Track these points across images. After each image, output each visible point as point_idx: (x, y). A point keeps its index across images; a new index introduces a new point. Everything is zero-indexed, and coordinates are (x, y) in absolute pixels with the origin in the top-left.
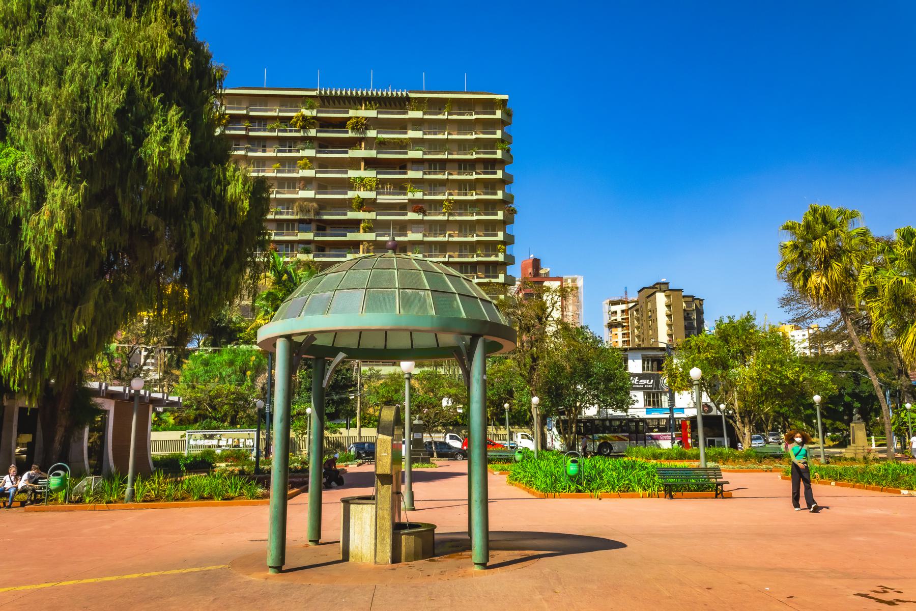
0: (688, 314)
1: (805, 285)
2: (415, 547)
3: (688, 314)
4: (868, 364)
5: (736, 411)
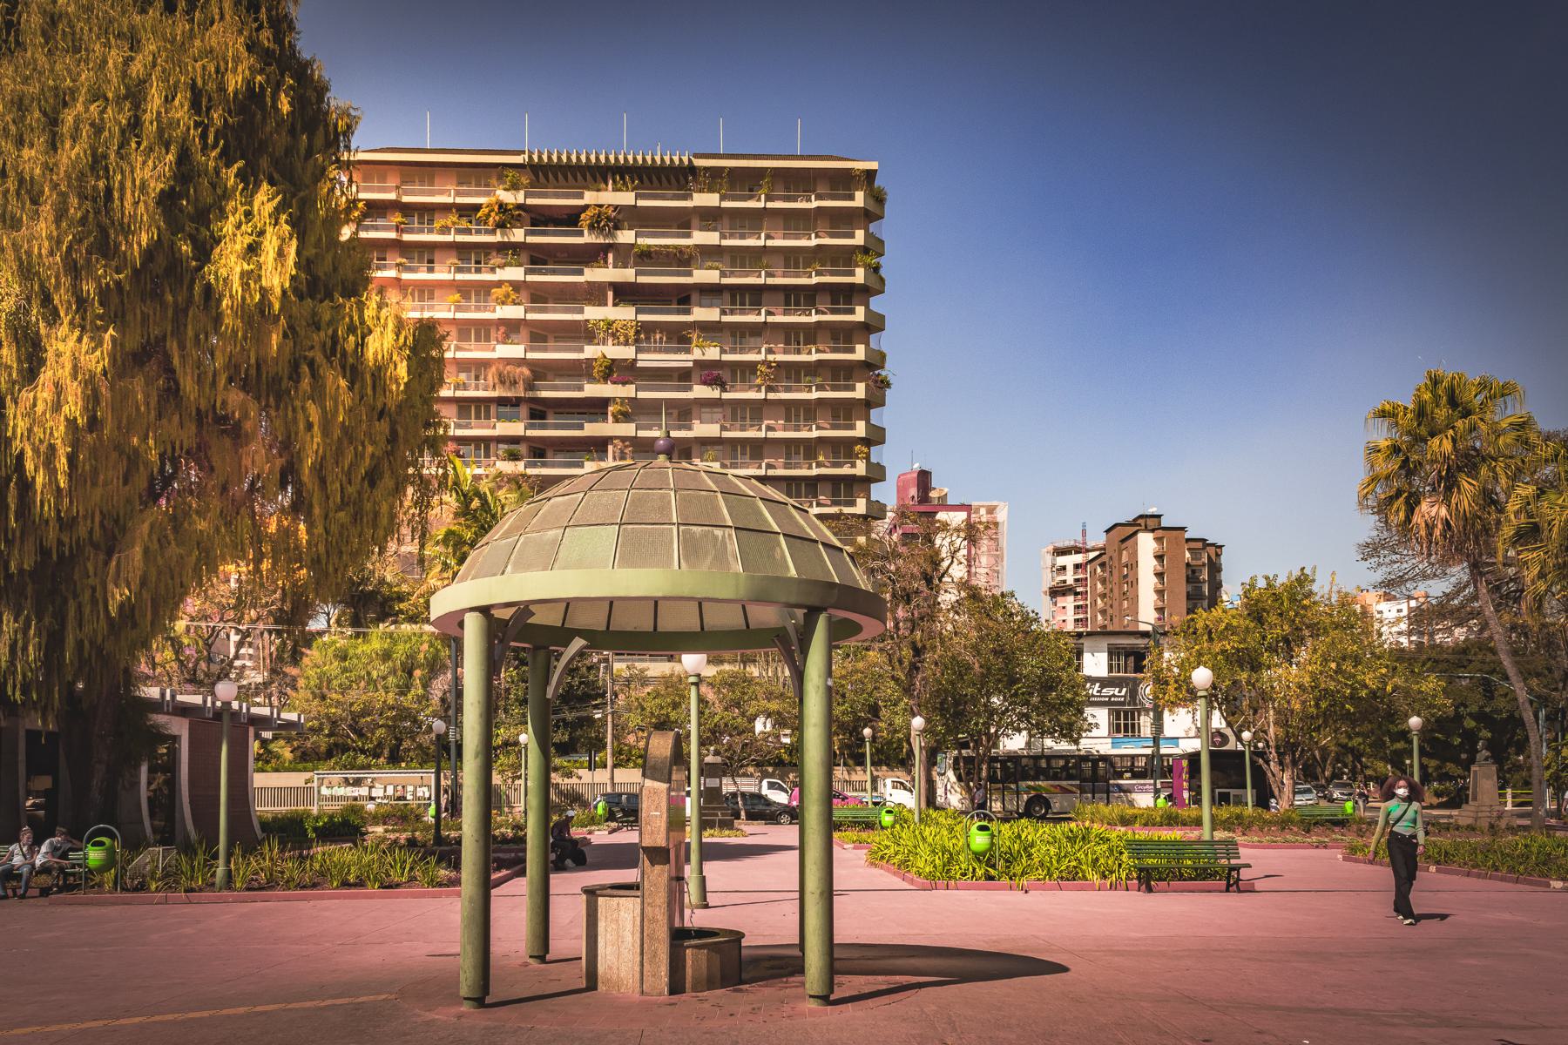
0: (1194, 572)
1: (1408, 519)
2: (708, 967)
3: (1194, 572)
5: (1271, 744)
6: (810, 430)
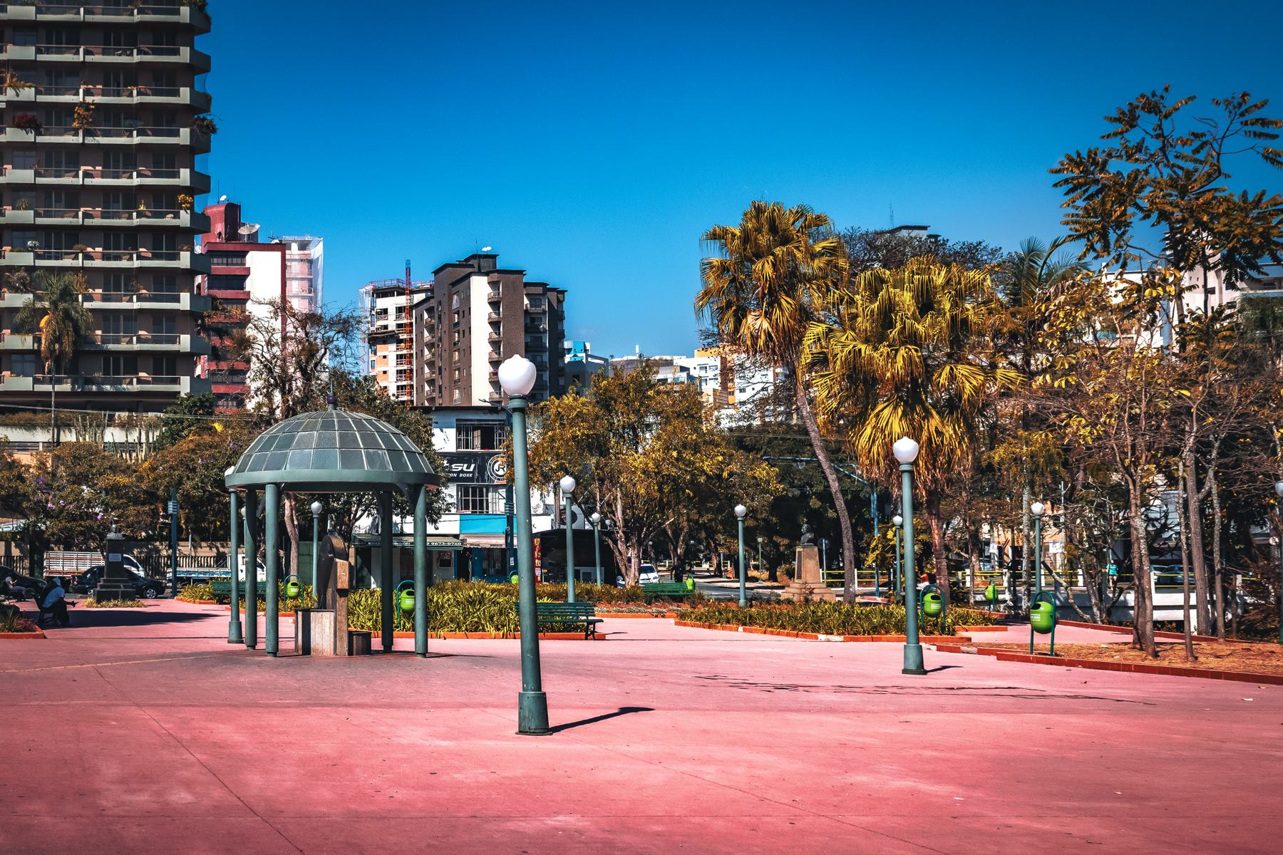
0: (533, 320)
1: (737, 330)
3: (533, 320)
4: (825, 457)
5: (618, 524)
6: (131, 177)
